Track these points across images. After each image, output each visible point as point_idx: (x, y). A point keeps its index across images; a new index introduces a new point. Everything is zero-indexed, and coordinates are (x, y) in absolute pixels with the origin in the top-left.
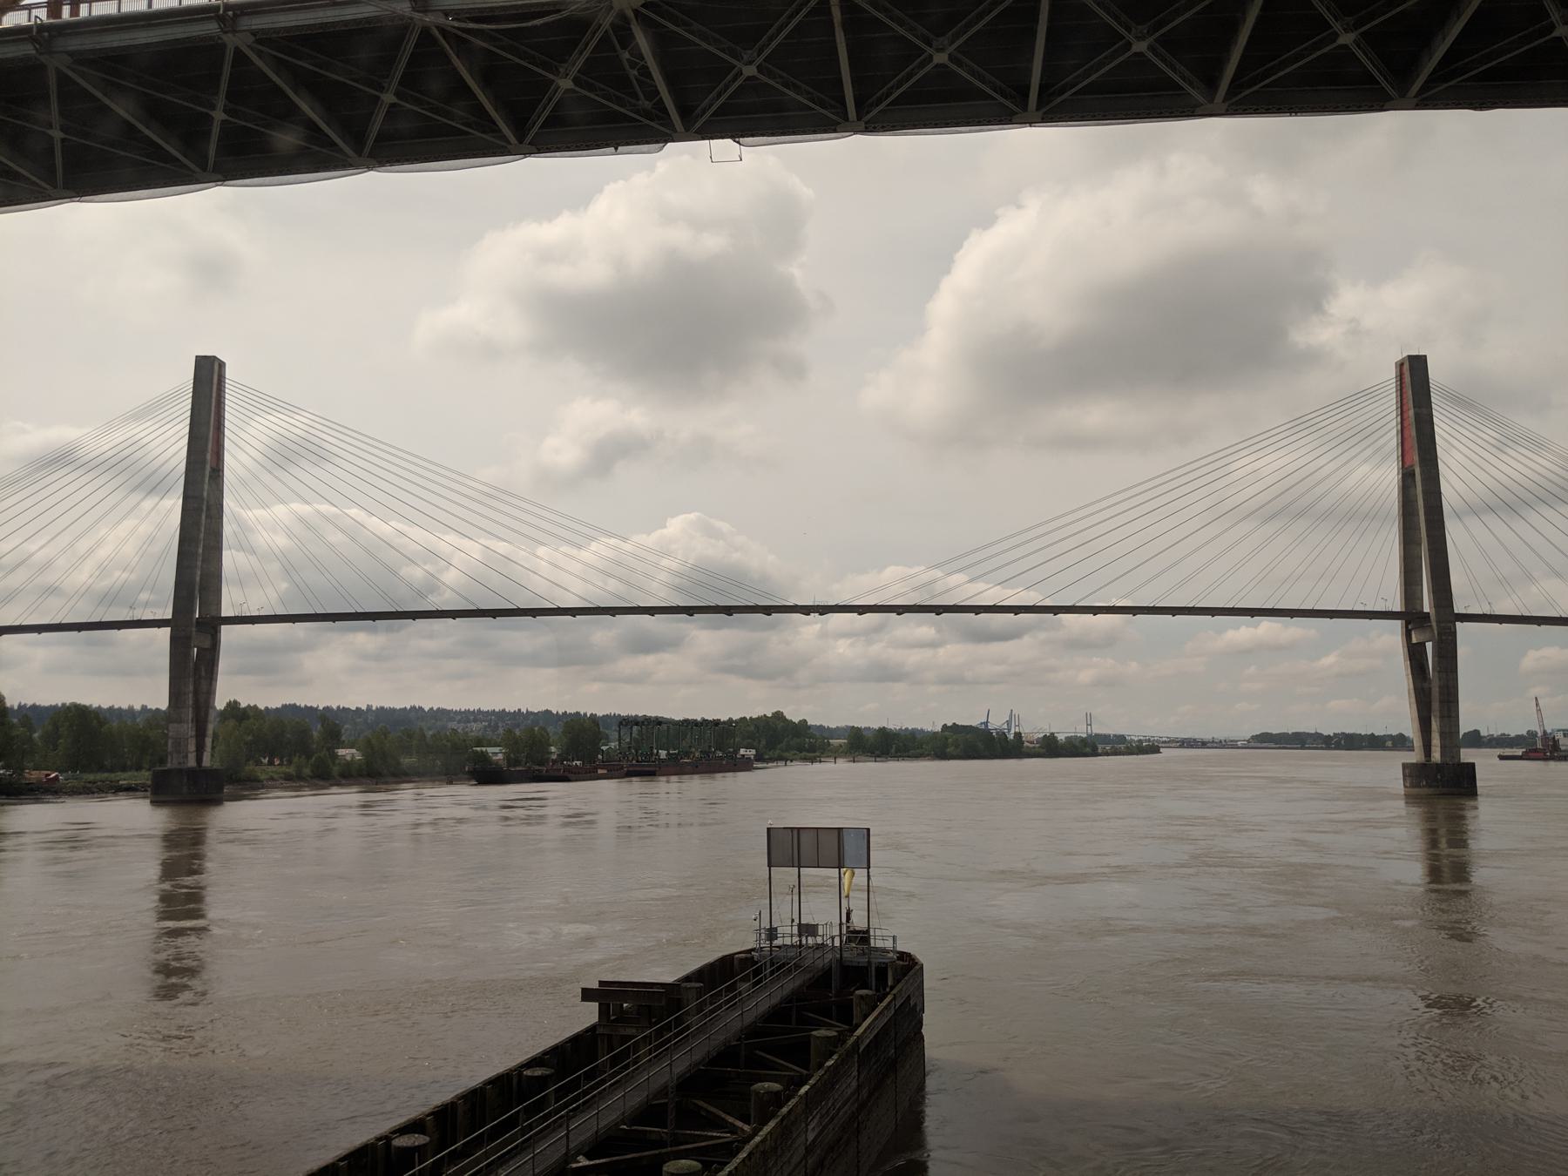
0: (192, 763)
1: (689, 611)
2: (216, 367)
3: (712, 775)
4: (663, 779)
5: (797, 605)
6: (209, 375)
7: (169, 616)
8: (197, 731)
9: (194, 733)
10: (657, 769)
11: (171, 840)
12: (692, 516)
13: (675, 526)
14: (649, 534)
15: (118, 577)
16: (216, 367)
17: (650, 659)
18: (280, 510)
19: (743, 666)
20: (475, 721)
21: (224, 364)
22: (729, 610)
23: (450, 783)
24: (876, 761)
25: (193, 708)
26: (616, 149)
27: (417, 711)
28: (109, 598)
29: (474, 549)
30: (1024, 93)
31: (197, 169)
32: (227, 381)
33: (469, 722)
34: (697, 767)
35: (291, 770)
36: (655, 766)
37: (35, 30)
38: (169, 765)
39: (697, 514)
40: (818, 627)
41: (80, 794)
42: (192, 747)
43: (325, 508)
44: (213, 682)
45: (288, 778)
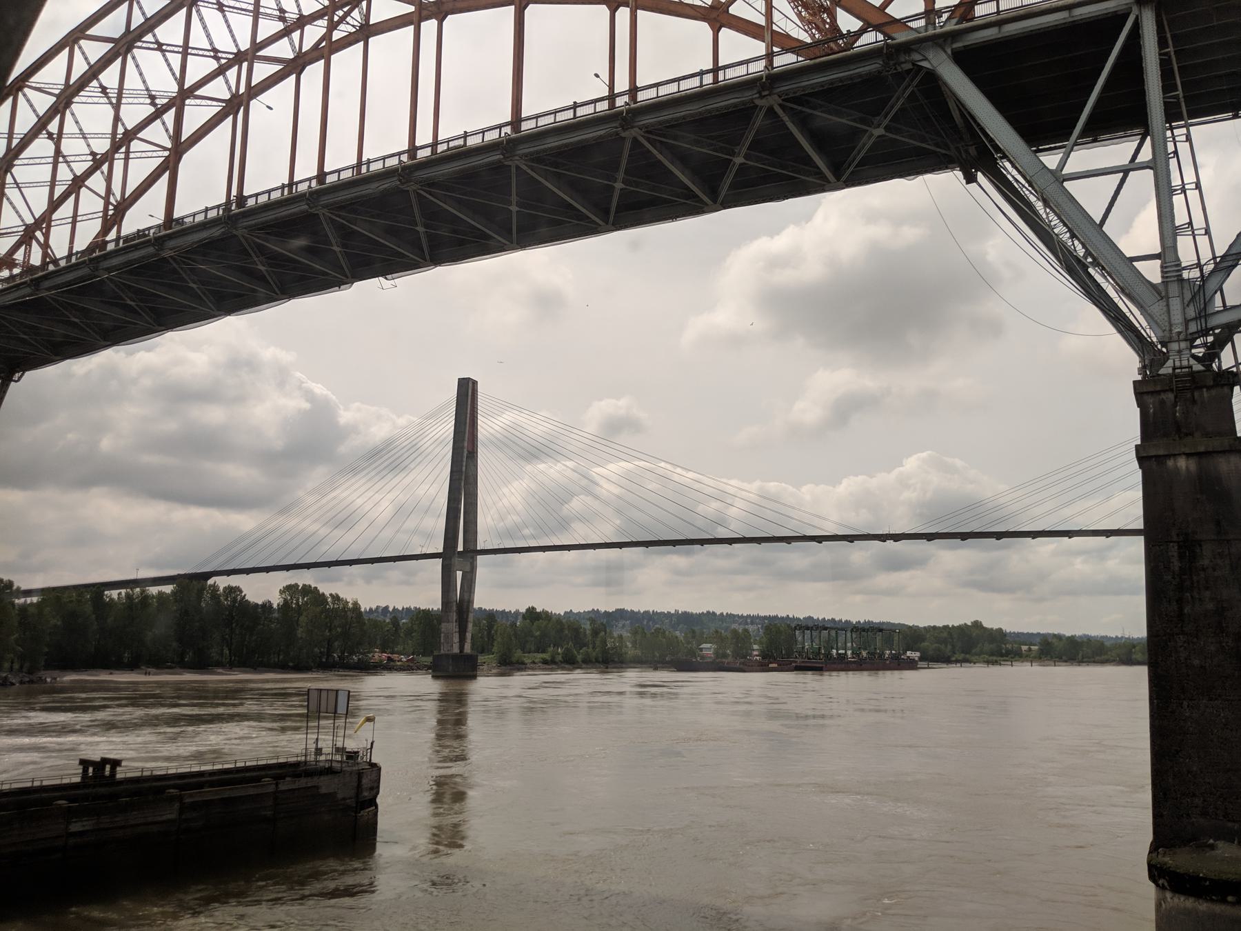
0: (456, 650)
1: (930, 537)
2: (470, 385)
3: (876, 672)
4: (827, 673)
5: (870, 534)
6: (467, 391)
7: (441, 550)
8: (459, 628)
9: (457, 630)
10: (824, 665)
11: (444, 698)
12: (924, 455)
13: (911, 464)
14: (889, 472)
15: (513, 519)
16: (470, 385)
17: (902, 577)
18: (612, 467)
19: (988, 583)
20: (752, 623)
21: (477, 382)
22: (964, 536)
23: (656, 669)
24: (1055, 666)
25: (457, 613)
26: (340, 287)
27: (776, 617)
28: (509, 534)
29: (755, 486)
30: (607, 212)
31: (507, 243)
32: (479, 393)
33: (747, 624)
34: (861, 665)
35: (546, 656)
36: (822, 663)
37: (505, 143)
38: (442, 652)
39: (929, 452)
40: (1055, 545)
41: (405, 670)
42: (456, 639)
43: (642, 464)
44: (472, 595)
45: (545, 662)
